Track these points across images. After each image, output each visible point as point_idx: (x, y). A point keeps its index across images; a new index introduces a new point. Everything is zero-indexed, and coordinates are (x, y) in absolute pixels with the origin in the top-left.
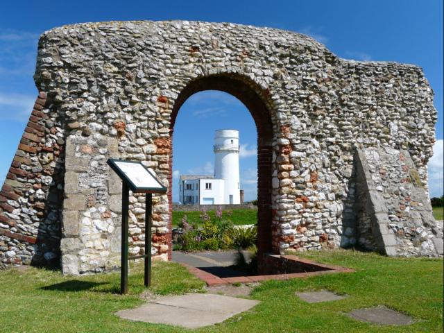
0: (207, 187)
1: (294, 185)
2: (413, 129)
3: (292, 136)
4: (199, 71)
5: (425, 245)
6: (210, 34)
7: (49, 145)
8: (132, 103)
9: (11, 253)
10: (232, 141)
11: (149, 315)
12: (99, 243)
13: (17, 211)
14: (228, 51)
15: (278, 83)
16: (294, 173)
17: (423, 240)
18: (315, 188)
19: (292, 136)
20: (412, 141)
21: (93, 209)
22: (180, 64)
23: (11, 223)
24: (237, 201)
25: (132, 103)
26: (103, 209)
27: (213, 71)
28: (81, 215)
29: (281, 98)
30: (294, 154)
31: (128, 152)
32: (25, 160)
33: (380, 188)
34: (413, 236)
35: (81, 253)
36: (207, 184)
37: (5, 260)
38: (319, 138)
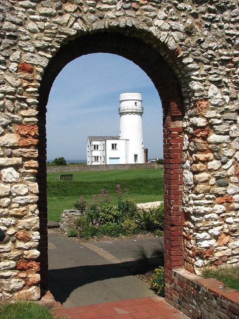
0: (113, 148)
1: (213, 181)
3: (211, 114)
10: (136, 103)
19: (211, 114)
22: (50, 15)
29: (197, 61)
30: (213, 138)
36: (113, 145)
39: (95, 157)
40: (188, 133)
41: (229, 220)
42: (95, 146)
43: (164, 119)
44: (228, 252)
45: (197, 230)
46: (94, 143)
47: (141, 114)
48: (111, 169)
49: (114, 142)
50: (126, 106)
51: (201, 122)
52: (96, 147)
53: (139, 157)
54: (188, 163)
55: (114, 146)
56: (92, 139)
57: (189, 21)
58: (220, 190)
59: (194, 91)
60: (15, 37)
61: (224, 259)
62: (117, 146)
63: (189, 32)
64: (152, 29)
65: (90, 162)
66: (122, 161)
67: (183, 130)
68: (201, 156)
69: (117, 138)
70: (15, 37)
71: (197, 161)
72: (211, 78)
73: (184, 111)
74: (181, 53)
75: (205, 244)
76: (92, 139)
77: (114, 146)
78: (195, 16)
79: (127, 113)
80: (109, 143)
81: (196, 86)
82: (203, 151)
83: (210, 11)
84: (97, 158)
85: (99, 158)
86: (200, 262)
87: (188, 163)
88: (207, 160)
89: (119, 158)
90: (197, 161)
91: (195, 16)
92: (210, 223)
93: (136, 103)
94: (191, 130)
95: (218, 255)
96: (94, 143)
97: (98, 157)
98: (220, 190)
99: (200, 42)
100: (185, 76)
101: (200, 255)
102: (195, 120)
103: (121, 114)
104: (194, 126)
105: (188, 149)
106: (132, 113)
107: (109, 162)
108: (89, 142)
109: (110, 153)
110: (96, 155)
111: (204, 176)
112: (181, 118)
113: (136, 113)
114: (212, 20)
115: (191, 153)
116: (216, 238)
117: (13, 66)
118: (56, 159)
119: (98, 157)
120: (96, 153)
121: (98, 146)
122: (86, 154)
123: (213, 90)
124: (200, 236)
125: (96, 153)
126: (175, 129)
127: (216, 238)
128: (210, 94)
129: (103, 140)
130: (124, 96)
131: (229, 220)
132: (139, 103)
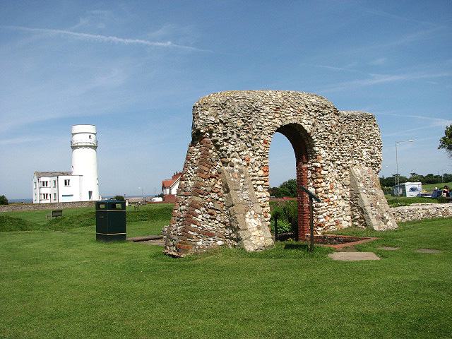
0: (66, 184)
1: (323, 192)
2: (372, 154)
3: (322, 161)
4: (280, 123)
5: (389, 223)
6: (282, 99)
7: (214, 173)
8: (253, 145)
9: (200, 243)
10: (90, 136)
11: (414, 255)
12: (257, 233)
13: (200, 216)
14: (292, 109)
15: (314, 129)
16: (323, 184)
17: (388, 221)
18: (333, 193)
19: (322, 161)
20: (373, 161)
21: (249, 213)
22: (271, 119)
23: (198, 224)
24: (95, 198)
25: (253, 145)
26: (253, 213)
27: (287, 123)
28: (245, 218)
29: (317, 138)
30: (323, 172)
31: (253, 176)
32: (202, 184)
33: (364, 191)
34: (383, 218)
35: (251, 238)
36: (66, 181)
37: (197, 247)
38: (333, 161)
39: (44, 195)
40: (311, 170)
41: (329, 209)
42: (44, 182)
43: (297, 164)
44: (329, 224)
45: (318, 214)
46: (43, 179)
47: (95, 147)
48: (68, 207)
49: (67, 178)
50: (78, 139)
51: (319, 165)
52: (45, 184)
53: (93, 194)
54: (311, 184)
55: (66, 183)
56: (40, 175)
57: (314, 120)
58: (326, 196)
59: (315, 152)
60: (261, 129)
61: (327, 228)
62: (70, 183)
63: (313, 125)
64: (302, 124)
65: (36, 200)
66: (75, 199)
67: (308, 169)
68: (319, 181)
69: (68, 174)
70: (261, 129)
71: (318, 182)
72: (322, 145)
73: (308, 159)
74: (312, 135)
75: (322, 220)
76: (40, 175)
77: (66, 183)
78: (315, 118)
79: (81, 147)
80: (62, 179)
81: (317, 149)
82: (319, 178)
83: (319, 115)
84: (46, 196)
85: (49, 195)
86: (320, 229)
87: (311, 184)
88: (321, 182)
89: (72, 195)
90: (318, 182)
91: (315, 118)
92: (323, 210)
93: (90, 136)
94: (314, 169)
95: (326, 225)
96: (43, 179)
97: (47, 194)
98: (326, 196)
99: (317, 129)
100: (311, 144)
101: (320, 226)
102: (316, 164)
103: (74, 148)
104: (316, 167)
105: (311, 178)
106: (86, 146)
107: (62, 200)
108: (36, 178)
109: (63, 190)
110: (45, 193)
111: (320, 189)
112: (306, 163)
113: (91, 147)
114: (320, 120)
115: (313, 179)
116: (325, 217)
117: (262, 141)
118: (117, 197)
119: (47, 194)
120: (45, 190)
121: (47, 182)
122: (32, 191)
123: (322, 151)
124: (319, 216)
125: (45, 190)
126: (304, 168)
127: (325, 217)
128: (321, 152)
129: (53, 176)
130: (77, 129)
131: (329, 209)
132: (93, 136)
